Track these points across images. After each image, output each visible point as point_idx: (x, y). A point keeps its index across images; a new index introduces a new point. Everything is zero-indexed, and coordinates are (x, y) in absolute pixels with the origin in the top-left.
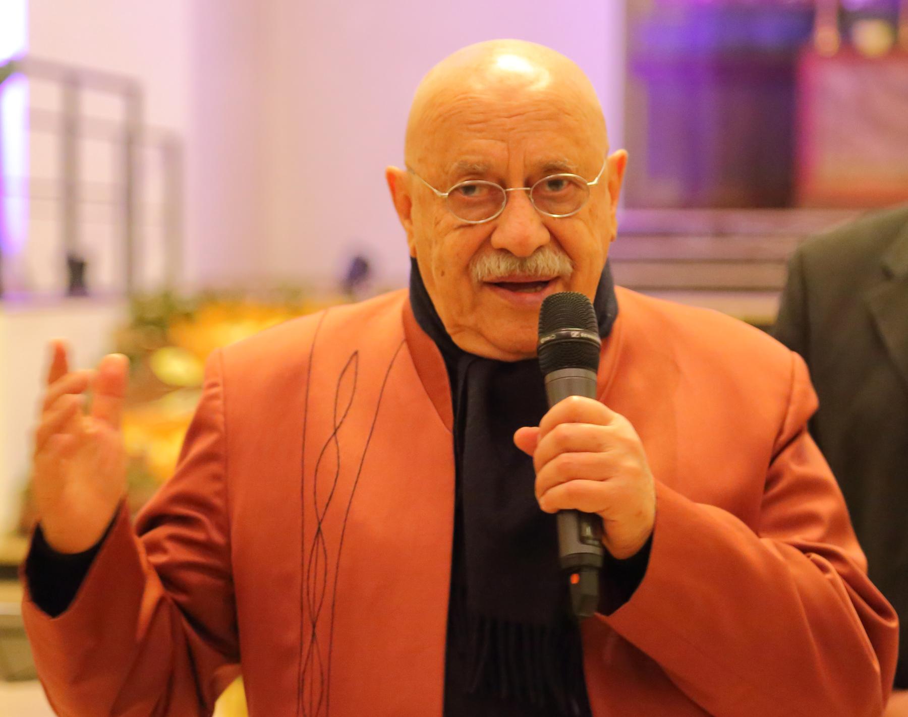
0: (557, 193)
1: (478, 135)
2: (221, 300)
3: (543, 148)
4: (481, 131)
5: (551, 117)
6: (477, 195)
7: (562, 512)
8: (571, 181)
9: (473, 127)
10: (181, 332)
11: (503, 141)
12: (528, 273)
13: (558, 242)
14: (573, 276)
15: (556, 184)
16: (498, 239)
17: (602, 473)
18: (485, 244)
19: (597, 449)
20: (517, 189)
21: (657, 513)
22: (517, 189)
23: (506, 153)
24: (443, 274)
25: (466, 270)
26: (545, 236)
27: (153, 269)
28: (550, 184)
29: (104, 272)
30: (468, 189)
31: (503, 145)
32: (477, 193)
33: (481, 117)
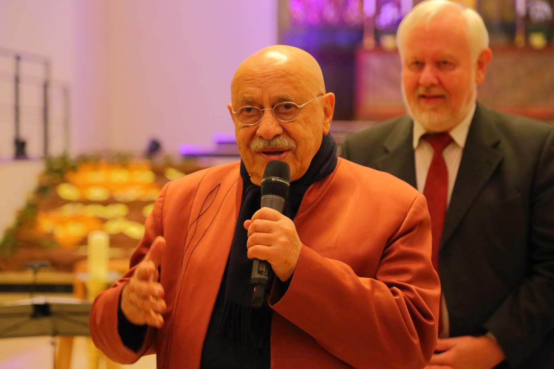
0: (289, 110)
1: (250, 85)
2: (90, 161)
3: (277, 90)
4: (251, 83)
5: (282, 77)
6: (251, 113)
7: (256, 259)
8: (294, 106)
9: (248, 82)
10: (71, 176)
11: (260, 88)
12: (272, 147)
13: (286, 132)
14: (297, 148)
15: (288, 106)
16: (258, 132)
17: (268, 242)
18: (253, 135)
19: (269, 231)
20: (267, 110)
21: (299, 261)
22: (267, 110)
23: (261, 93)
24: (240, 148)
25: (248, 146)
26: (279, 130)
27: (56, 149)
28: (283, 107)
29: (34, 148)
30: (249, 110)
31: (260, 89)
32: (253, 111)
33: (251, 78)
